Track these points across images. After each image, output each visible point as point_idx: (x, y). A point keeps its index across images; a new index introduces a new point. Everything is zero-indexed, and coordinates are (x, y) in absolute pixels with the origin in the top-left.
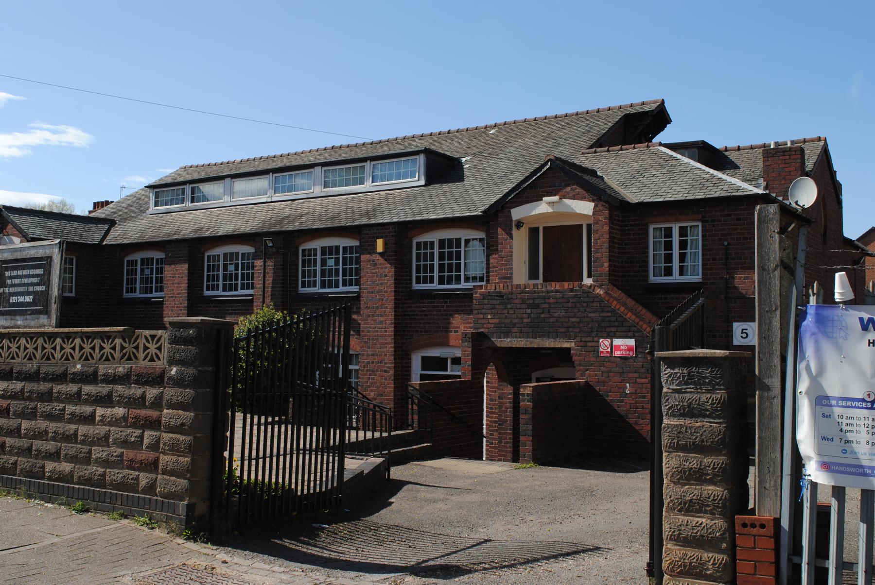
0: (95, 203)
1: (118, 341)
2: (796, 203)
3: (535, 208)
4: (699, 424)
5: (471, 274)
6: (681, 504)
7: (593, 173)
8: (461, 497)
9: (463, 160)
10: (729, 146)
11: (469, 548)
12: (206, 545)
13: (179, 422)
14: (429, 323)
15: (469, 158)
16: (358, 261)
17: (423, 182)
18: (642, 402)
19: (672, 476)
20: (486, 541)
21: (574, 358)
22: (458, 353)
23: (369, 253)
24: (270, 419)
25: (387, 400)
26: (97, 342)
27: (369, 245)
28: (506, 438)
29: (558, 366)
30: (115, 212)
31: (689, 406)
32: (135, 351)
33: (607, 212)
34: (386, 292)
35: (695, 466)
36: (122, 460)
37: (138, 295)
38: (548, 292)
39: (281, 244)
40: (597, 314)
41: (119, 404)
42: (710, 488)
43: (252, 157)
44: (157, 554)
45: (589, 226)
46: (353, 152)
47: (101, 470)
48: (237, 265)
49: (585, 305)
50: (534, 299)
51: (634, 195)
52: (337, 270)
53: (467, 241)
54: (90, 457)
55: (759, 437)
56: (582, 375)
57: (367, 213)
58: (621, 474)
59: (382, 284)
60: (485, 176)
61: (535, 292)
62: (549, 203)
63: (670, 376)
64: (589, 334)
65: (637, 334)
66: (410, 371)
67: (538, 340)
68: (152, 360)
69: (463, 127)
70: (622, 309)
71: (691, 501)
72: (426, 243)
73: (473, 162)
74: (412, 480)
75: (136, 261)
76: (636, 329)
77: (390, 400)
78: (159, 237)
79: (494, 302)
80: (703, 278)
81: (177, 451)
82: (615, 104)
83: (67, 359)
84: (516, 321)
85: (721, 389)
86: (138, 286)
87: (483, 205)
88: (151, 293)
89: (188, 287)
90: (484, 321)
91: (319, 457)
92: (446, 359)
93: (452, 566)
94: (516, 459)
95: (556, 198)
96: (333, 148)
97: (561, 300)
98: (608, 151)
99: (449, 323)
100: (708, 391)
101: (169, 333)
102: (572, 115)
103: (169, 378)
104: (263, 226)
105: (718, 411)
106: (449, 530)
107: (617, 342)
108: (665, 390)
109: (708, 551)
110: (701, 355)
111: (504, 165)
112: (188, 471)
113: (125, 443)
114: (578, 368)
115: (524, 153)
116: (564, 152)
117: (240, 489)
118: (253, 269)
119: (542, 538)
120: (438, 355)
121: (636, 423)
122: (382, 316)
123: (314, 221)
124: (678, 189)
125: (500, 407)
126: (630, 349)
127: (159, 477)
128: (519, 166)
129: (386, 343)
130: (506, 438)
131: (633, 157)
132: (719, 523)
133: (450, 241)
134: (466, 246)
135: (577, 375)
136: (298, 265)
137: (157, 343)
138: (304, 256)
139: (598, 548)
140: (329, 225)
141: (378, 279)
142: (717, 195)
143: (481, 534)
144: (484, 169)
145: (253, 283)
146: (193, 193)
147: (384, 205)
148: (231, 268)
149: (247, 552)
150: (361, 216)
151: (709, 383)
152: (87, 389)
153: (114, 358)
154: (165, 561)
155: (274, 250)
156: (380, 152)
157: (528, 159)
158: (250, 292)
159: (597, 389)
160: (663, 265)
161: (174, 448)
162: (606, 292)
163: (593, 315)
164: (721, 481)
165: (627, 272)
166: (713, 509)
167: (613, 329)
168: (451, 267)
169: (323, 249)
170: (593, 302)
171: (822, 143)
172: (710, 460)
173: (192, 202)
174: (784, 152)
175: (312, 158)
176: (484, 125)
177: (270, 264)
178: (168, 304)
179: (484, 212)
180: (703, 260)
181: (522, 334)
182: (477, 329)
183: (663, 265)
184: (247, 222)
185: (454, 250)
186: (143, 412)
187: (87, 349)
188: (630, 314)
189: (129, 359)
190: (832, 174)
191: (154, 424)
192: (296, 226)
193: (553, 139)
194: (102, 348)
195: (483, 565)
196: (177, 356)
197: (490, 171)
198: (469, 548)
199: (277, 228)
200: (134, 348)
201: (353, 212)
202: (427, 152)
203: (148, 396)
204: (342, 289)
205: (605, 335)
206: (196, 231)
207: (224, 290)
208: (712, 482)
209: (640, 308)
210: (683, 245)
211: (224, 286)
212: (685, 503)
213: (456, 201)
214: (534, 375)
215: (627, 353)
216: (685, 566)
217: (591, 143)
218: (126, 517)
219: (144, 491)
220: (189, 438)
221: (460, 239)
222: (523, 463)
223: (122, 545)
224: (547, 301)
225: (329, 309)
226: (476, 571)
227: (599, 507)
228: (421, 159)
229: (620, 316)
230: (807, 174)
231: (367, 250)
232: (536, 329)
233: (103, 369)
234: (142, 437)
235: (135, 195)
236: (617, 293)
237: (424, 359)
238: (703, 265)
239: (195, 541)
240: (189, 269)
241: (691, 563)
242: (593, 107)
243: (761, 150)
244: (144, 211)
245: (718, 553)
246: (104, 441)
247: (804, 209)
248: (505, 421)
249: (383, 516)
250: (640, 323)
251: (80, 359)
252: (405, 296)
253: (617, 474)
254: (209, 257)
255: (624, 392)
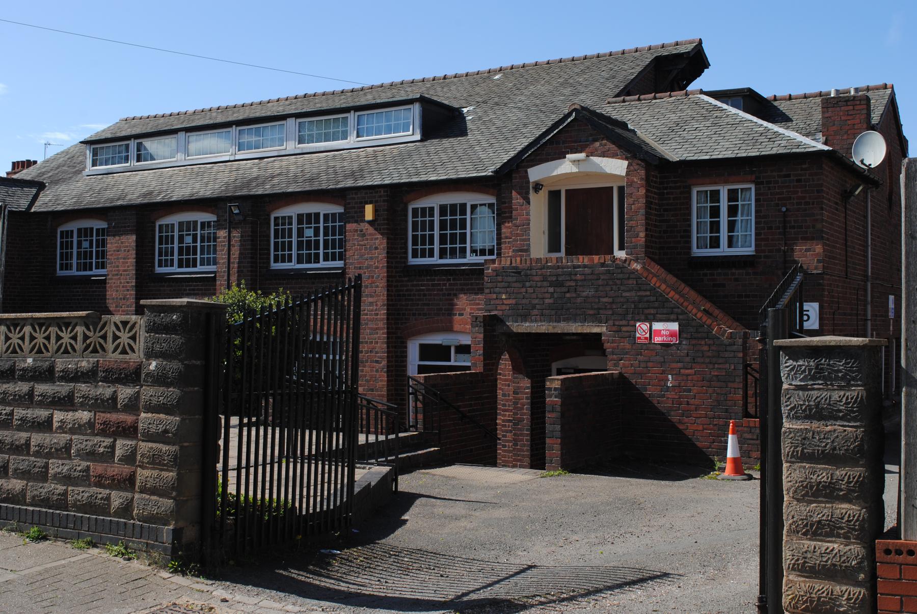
0: (14, 163)
1: (80, 329)
2: (862, 162)
3: (556, 168)
4: (829, 428)
5: (479, 246)
6: (806, 525)
7: (624, 125)
8: (482, 511)
9: (465, 110)
10: (779, 94)
11: (512, 576)
12: (198, 580)
13: (161, 428)
14: (428, 305)
15: (471, 108)
16: (342, 231)
17: (418, 137)
18: (687, 397)
19: (795, 492)
20: (530, 567)
21: (606, 345)
22: (466, 340)
23: (356, 222)
24: (246, 420)
25: (379, 396)
26: (53, 330)
27: (356, 212)
28: (522, 440)
29: (583, 355)
30: (43, 174)
31: (817, 405)
32: (102, 341)
33: (643, 173)
34: (377, 267)
35: (825, 479)
36: (88, 476)
37: (74, 272)
38: (575, 267)
39: (249, 212)
40: (633, 294)
41: (83, 406)
42: (843, 506)
43: (207, 107)
44: (139, 592)
45: (621, 189)
46: (330, 102)
47: (61, 488)
48: (317, 230)
49: (618, 282)
50: (557, 275)
51: (674, 152)
52: (317, 243)
53: (474, 207)
54: (47, 472)
55: (906, 444)
56: (616, 365)
57: (353, 173)
58: (667, 482)
59: (371, 258)
60: (493, 129)
61: (558, 267)
62: (574, 161)
63: (792, 369)
64: (624, 316)
65: (681, 317)
66: (406, 361)
67: (562, 324)
68: (124, 352)
69: (462, 71)
70: (663, 287)
71: (819, 522)
72: (423, 209)
73: (476, 113)
74: (423, 492)
75: (72, 232)
76: (679, 311)
77: (382, 396)
78: (99, 203)
79: (510, 279)
80: (756, 251)
81: (159, 464)
82: (643, 44)
83: (14, 352)
84: (536, 301)
85: (858, 386)
86: (74, 261)
87: (493, 164)
88: (91, 269)
89: (136, 262)
90: (497, 302)
91: (313, 466)
92: (449, 347)
93: (503, 601)
94: (538, 462)
95: (582, 156)
96: (305, 96)
97: (590, 277)
98: (639, 100)
99: (453, 305)
100: (841, 388)
101: (145, 318)
102: (592, 57)
103: (147, 375)
104: (227, 190)
105: (854, 412)
106: (482, 554)
107: (657, 326)
108: (785, 386)
109: (840, 583)
110: (833, 344)
111: (514, 115)
112: (173, 488)
113: (91, 455)
114: (610, 357)
115: (538, 102)
116: (587, 100)
117: (236, 509)
118: (215, 241)
119: (597, 563)
120: (439, 342)
121: (680, 422)
122: (371, 296)
123: (289, 183)
124: (727, 144)
125: (515, 403)
126: (672, 334)
127: (137, 496)
128: (533, 118)
129: (377, 329)
130: (522, 440)
131: (670, 107)
132: (854, 550)
133: (453, 206)
134: (472, 213)
135: (610, 364)
136: (269, 236)
137: (130, 330)
138: (276, 224)
139: (666, 575)
140: (308, 188)
141: (367, 254)
142: (774, 151)
143: (522, 559)
144: (490, 121)
145: (215, 259)
146: (138, 150)
147: (372, 164)
148: (188, 240)
149: (249, 587)
150: (346, 177)
151: (843, 378)
152: (41, 388)
153: (74, 350)
154: (150, 601)
155: (241, 218)
156: (363, 101)
157: (543, 109)
158: (212, 268)
159: (633, 381)
160: (709, 235)
161: (155, 461)
162: (643, 267)
163: (627, 294)
164: (857, 498)
165: (667, 241)
166: (848, 532)
167: (652, 311)
168: (454, 240)
169: (300, 217)
170: (629, 278)
171: (889, 91)
172: (844, 472)
173: (138, 160)
174: (847, 101)
175: (281, 109)
176: (486, 68)
177: (236, 234)
178: (112, 283)
179: (496, 172)
180: (756, 228)
181: (543, 317)
182: (489, 311)
183: (709, 235)
184: (207, 184)
185: (458, 217)
186: (114, 417)
187: (40, 338)
188: (672, 293)
189: (95, 351)
190: (899, 126)
191: (130, 431)
192: (267, 189)
193: (571, 85)
194: (59, 338)
195: (538, 598)
196: (157, 348)
197: (499, 123)
198: (512, 576)
199: (244, 192)
200: (101, 337)
201: (335, 173)
202: (423, 100)
203: (121, 397)
204: (322, 264)
205: (643, 318)
206: (145, 195)
207: (180, 266)
208: (846, 499)
209: (683, 285)
210: (733, 211)
211: (180, 261)
212: (812, 525)
213: (460, 159)
214: (555, 366)
215: (669, 339)
216: (812, 602)
217: (617, 91)
218: (95, 546)
219: (117, 514)
220: (173, 448)
221: (465, 204)
222: (550, 470)
223: (95, 581)
224: (573, 277)
225: (337, 288)
226: (532, 606)
227: (652, 523)
228: (417, 108)
229: (661, 295)
230: (873, 128)
231: (353, 217)
232: (560, 311)
233: (61, 363)
234: (113, 447)
235: (66, 152)
236: (655, 268)
237: (423, 347)
238: (756, 234)
239: (184, 574)
240: (137, 241)
241: (819, 598)
242: (617, 48)
243: (819, 100)
244: (80, 172)
245: (854, 586)
246: (65, 451)
247: (870, 169)
248: (522, 420)
249: (398, 538)
250: (685, 304)
251: (31, 351)
252: (399, 271)
253: (663, 482)
254: (161, 226)
255: (665, 385)
